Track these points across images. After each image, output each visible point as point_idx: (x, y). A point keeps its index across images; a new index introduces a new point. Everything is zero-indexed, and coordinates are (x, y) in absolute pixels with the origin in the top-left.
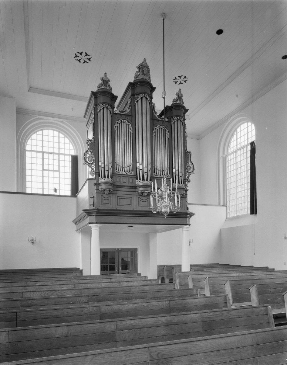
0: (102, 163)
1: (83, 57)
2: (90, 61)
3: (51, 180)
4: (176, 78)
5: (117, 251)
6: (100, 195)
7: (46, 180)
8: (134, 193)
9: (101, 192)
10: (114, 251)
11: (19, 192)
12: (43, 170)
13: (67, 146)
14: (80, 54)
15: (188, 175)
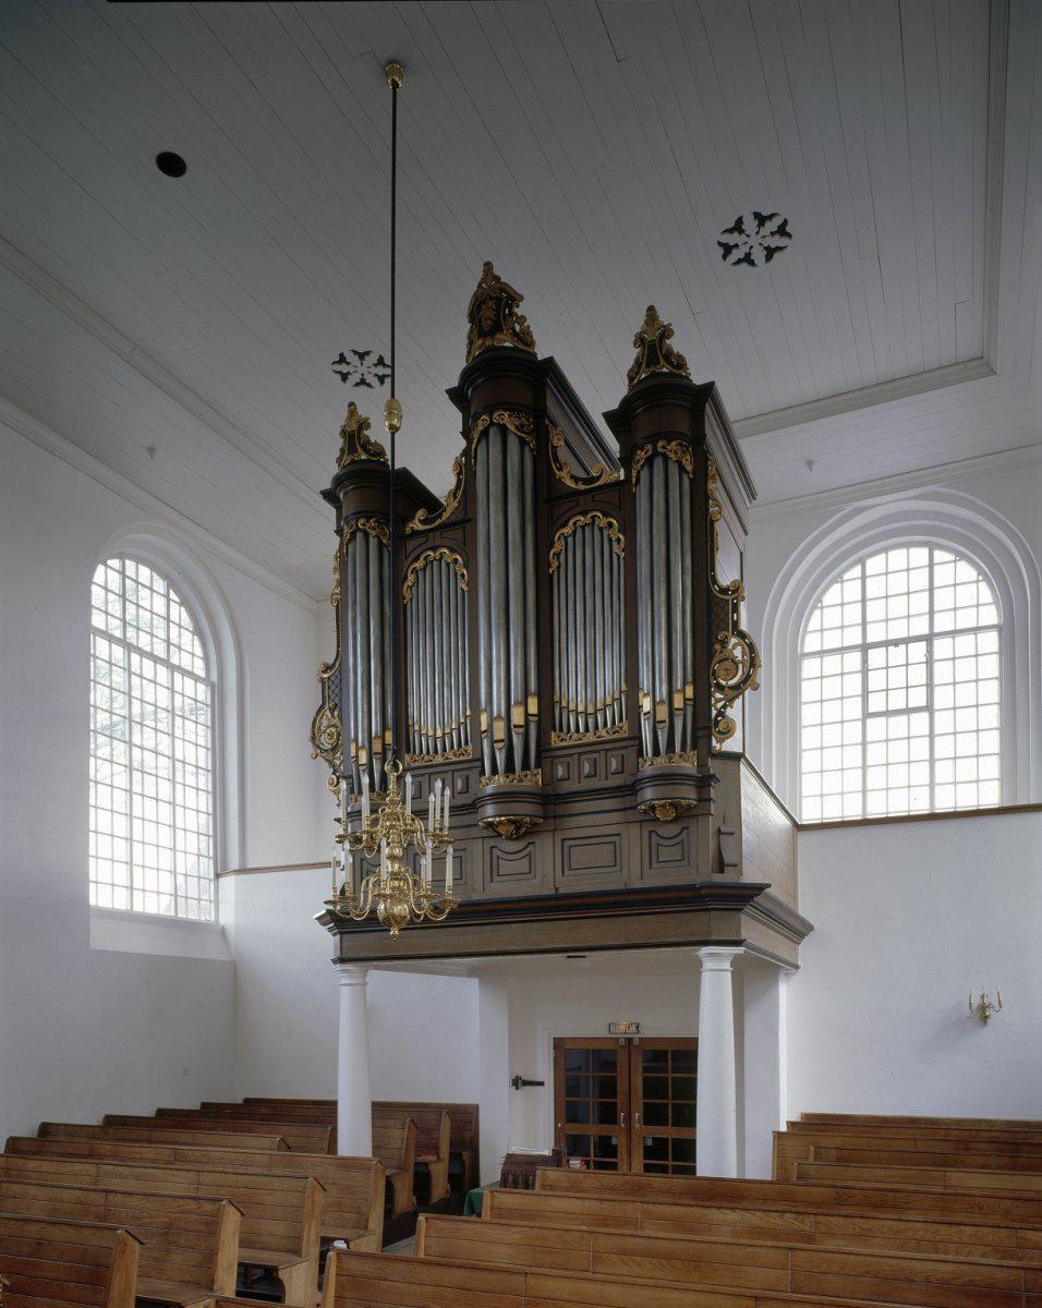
0: (363, 747)
1: (754, 240)
2: (790, 236)
3: (898, 751)
4: (342, 359)
5: (623, 1047)
6: (647, 828)
7: (876, 754)
8: (475, 832)
9: (645, 818)
10: (611, 1047)
11: (1021, 802)
12: (867, 715)
13: (967, 595)
14: (736, 234)
15: (719, 705)
